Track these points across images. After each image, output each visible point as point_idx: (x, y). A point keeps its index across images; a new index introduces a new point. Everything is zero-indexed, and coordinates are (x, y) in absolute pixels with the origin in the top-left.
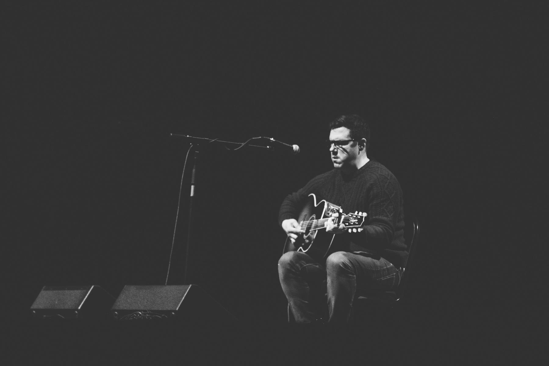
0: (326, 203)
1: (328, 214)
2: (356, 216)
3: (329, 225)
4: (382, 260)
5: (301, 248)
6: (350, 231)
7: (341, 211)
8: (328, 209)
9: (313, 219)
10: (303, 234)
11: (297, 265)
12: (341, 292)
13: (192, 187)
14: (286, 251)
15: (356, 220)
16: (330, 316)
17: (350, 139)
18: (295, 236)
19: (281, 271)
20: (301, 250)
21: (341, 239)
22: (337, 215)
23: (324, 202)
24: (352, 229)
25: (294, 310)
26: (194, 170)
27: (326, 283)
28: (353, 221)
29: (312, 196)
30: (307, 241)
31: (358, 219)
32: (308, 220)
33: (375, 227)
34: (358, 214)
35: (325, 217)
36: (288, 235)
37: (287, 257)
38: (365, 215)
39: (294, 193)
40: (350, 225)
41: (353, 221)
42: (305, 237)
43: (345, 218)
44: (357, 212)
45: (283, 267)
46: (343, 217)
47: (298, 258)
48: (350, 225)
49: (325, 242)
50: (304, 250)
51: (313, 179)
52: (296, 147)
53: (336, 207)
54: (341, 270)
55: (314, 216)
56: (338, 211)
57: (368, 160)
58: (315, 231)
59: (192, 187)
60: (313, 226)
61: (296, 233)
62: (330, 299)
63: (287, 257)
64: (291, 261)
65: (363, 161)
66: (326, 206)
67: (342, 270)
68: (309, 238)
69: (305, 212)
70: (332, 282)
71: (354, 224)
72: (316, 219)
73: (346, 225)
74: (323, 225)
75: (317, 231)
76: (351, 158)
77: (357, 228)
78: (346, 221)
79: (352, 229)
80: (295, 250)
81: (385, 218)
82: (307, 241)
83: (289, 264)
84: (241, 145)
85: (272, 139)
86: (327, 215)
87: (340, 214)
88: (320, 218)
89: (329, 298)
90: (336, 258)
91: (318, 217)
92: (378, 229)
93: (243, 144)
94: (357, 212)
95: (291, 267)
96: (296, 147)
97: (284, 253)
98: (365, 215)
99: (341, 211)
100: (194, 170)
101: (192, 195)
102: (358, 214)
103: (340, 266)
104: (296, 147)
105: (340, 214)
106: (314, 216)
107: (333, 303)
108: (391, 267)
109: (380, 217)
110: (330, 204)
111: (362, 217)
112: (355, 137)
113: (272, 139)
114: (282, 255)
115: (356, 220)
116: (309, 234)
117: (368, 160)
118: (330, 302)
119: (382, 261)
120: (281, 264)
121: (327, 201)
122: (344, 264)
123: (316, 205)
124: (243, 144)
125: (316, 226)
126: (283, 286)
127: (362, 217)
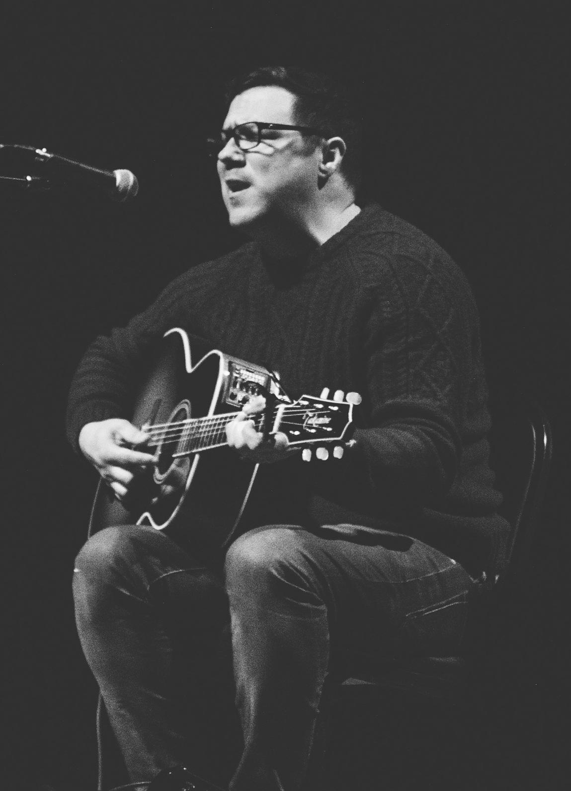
1: (233, 397)
2: (326, 405)
3: (240, 432)
6: (306, 455)
7: (275, 389)
9: (182, 415)
14: (95, 531)
15: (326, 420)
16: (248, 739)
18: (125, 475)
19: (82, 591)
20: (146, 522)
21: (272, 484)
23: (216, 358)
24: (313, 448)
25: (116, 723)
27: (230, 635)
28: (315, 421)
29: (178, 335)
30: (169, 489)
31: (331, 414)
32: (165, 420)
33: (393, 432)
34: (331, 396)
36: (103, 473)
37: (102, 544)
38: (353, 399)
39: (116, 331)
40: (305, 435)
41: (315, 421)
42: (158, 476)
43: (287, 412)
45: (91, 581)
46: (281, 408)
47: (140, 548)
48: (305, 435)
49: (233, 490)
52: (125, 178)
53: (258, 377)
54: (278, 584)
55: (186, 405)
56: (263, 390)
57: (354, 211)
58: (192, 457)
61: (127, 465)
63: (102, 544)
64: (118, 560)
66: (223, 372)
67: (278, 586)
68: (174, 479)
70: (246, 629)
71: (320, 432)
72: (193, 417)
73: (292, 438)
74: (223, 437)
75: (197, 457)
76: (287, 206)
77: (330, 447)
78: (292, 422)
79: (313, 448)
83: (111, 569)
85: (43, 152)
86: (229, 401)
87: (272, 402)
88: (206, 414)
89: (239, 684)
91: (200, 411)
95: (115, 577)
96: (123, 177)
97: (92, 534)
98: (353, 399)
99: (275, 389)
102: (331, 396)
103: (270, 574)
104: (123, 177)
105: (272, 402)
106: (186, 405)
108: (453, 572)
110: (239, 364)
111: (344, 408)
113: (43, 152)
114: (84, 540)
115: (326, 420)
116: (173, 466)
117: (354, 211)
119: (417, 555)
120: (86, 570)
121: (224, 352)
122: (283, 567)
123: (189, 369)
125: (194, 442)
127: (344, 408)
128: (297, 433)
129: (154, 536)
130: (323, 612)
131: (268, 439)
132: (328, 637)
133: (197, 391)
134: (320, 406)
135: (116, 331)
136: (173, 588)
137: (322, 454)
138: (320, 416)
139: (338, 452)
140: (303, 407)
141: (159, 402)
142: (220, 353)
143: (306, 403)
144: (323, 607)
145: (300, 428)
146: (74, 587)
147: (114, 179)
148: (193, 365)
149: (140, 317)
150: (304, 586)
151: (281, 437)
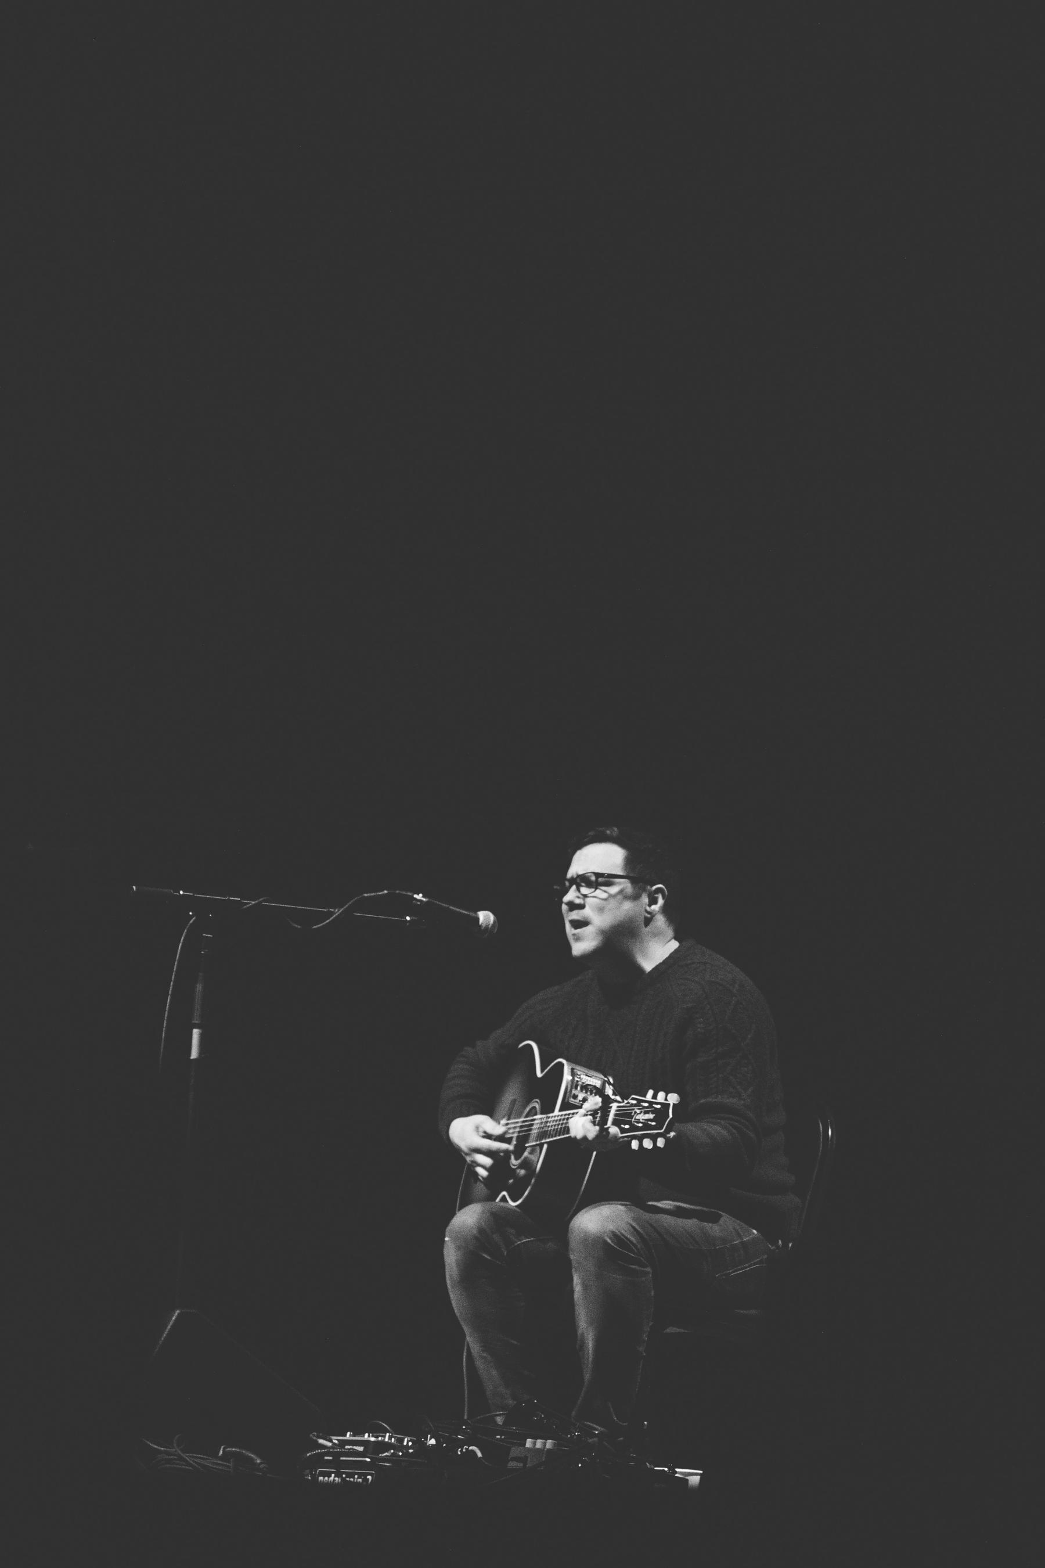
0: (567, 1069)
1: (575, 1097)
3: (581, 1126)
4: (726, 1220)
5: (504, 1193)
6: (635, 1145)
7: (609, 1091)
8: (574, 1085)
9: (533, 1112)
10: (507, 1152)
11: (496, 1237)
12: (612, 1314)
13: (196, 1032)
15: (651, 1116)
16: (587, 1377)
17: (621, 873)
18: (487, 1161)
19: (451, 1256)
20: (504, 1199)
21: (607, 1167)
22: (594, 1102)
23: (561, 1065)
24: (640, 1139)
26: (199, 987)
28: (642, 1117)
29: (530, 1046)
30: (522, 1172)
32: (519, 1116)
33: (705, 1126)
34: (655, 1097)
35: (565, 1106)
36: (468, 1159)
37: (468, 1218)
38: (673, 1098)
39: (479, 1043)
40: (634, 1128)
41: (642, 1117)
42: (514, 1162)
44: (651, 1093)
45: (459, 1248)
47: (499, 1220)
48: (634, 1128)
50: (514, 1201)
51: (520, 1011)
52: (487, 918)
53: (595, 1080)
54: (611, 1251)
55: (536, 1104)
56: (600, 1092)
57: (674, 945)
58: (541, 1146)
59: (196, 1032)
60: (535, 1132)
61: (489, 1153)
62: (583, 1334)
64: (481, 1230)
65: (656, 951)
66: (567, 1077)
68: (526, 1164)
69: (511, 1094)
70: (585, 1287)
71: (646, 1126)
72: (542, 1113)
73: (623, 1131)
74: (567, 1130)
75: (545, 1146)
76: (619, 940)
79: (640, 1139)
80: (492, 1198)
81: (733, 1101)
82: (522, 1172)
83: (476, 1238)
84: (332, 913)
85: (419, 897)
86: (572, 1100)
87: (607, 1101)
88: (553, 1111)
89: (580, 1332)
90: (594, 1221)
91: (548, 1109)
92: (716, 1130)
93: (338, 912)
94: (651, 1093)
95: (478, 1245)
96: (485, 917)
97: (460, 1208)
98: (673, 1098)
99: (609, 1091)
100: (199, 987)
101: (194, 1054)
102: (655, 1097)
103: (605, 1242)
104: (485, 917)
105: (607, 1101)
107: (590, 1344)
109: (719, 1099)
110: (580, 1070)
111: (665, 1106)
112: (639, 873)
113: (419, 897)
114: (453, 1214)
115: (651, 1116)
116: (526, 1154)
117: (674, 945)
118: (583, 1344)
119: (725, 1227)
120: (455, 1239)
122: (616, 1236)
123: (539, 1074)
124: (338, 912)
125: (543, 1134)
126: (456, 1298)
127: (665, 1106)
128: (627, 1127)
129: (510, 1211)
130: (648, 1273)
131: (603, 1131)
132: (653, 1293)
133: (545, 1092)
134: (646, 1105)
135: (479, 1043)
136: (526, 1254)
137: (648, 1144)
138: (646, 1113)
139: (661, 1142)
140: (632, 1105)
141: (514, 1101)
142: (564, 1061)
143: (634, 1102)
144: (649, 1269)
145: (629, 1123)
146: (445, 1253)
147: (478, 919)
148: (542, 1071)
149: (499, 1032)
150: (632, 1251)
151: (614, 1130)
